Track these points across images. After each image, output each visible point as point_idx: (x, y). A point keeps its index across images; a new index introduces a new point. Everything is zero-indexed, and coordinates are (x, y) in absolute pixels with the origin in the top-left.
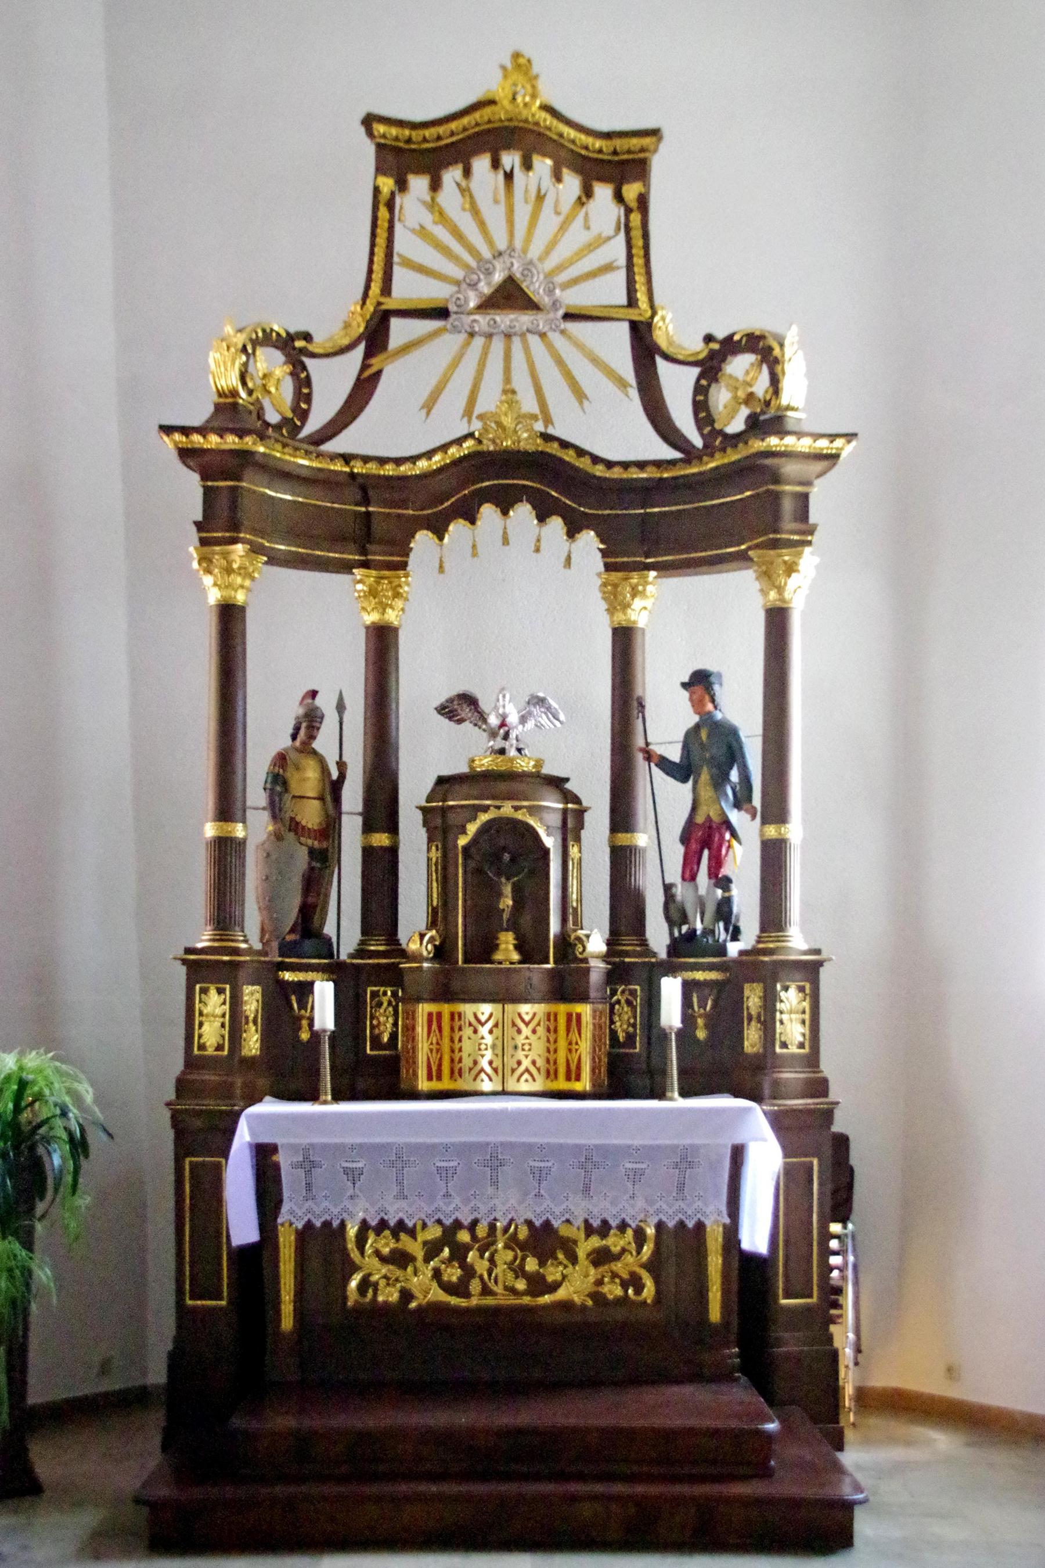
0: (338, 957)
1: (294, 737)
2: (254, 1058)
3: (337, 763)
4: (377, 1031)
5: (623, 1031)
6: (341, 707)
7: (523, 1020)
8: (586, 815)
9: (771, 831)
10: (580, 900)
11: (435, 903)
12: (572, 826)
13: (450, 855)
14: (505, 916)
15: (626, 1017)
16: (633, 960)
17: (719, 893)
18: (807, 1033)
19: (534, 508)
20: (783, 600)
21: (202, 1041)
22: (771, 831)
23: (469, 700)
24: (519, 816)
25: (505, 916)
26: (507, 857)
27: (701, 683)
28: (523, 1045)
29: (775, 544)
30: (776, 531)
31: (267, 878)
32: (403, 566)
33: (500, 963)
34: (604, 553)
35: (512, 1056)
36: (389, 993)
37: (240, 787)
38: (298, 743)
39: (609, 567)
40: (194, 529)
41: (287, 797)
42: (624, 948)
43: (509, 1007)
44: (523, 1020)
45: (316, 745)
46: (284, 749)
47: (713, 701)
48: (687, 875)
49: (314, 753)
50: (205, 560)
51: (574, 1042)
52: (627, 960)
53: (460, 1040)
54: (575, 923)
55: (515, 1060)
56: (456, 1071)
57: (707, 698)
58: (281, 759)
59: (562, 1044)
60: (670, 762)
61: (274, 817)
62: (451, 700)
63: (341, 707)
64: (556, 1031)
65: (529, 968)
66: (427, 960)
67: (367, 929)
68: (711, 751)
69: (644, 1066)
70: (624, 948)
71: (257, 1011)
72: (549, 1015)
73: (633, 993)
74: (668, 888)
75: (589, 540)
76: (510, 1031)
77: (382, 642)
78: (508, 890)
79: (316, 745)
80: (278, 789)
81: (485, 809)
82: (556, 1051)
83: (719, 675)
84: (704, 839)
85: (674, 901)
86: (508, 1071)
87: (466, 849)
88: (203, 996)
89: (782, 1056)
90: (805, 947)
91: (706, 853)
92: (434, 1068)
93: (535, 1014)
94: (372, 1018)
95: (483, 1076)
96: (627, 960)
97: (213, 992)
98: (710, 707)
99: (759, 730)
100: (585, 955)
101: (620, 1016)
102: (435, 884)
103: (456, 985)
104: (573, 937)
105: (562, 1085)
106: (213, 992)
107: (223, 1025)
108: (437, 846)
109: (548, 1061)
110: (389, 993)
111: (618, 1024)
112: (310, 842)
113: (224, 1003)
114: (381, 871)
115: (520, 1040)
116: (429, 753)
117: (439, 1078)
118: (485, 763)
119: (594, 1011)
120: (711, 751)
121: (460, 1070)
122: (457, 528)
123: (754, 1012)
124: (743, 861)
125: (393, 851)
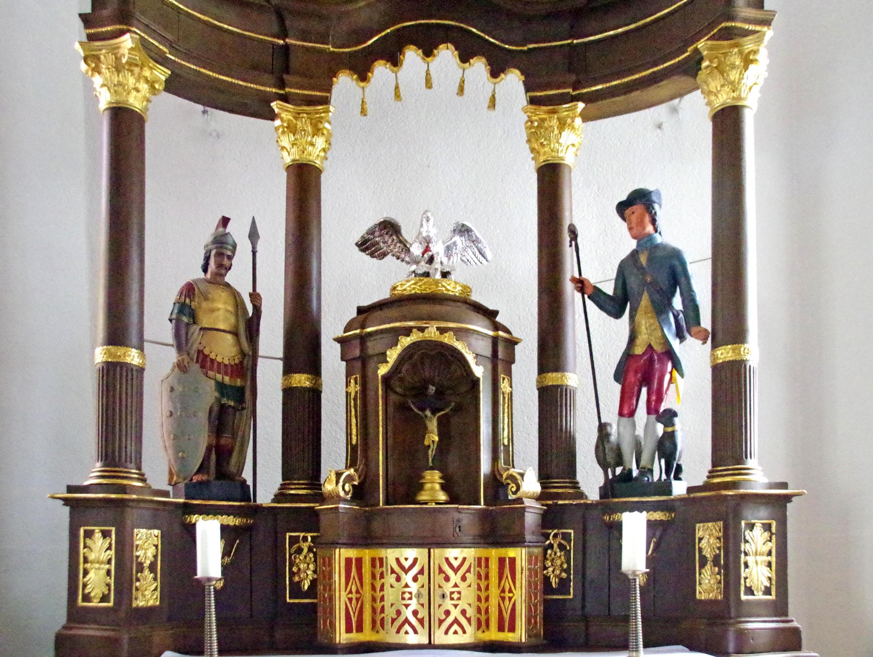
0: (255, 500)
1: (205, 269)
2: (151, 609)
3: (251, 295)
5: (556, 576)
6: (254, 235)
8: (517, 348)
9: (725, 354)
10: (511, 439)
11: (354, 442)
13: (370, 386)
14: (431, 453)
15: (559, 562)
17: (660, 429)
18: (773, 576)
20: (739, 98)
21: (87, 591)
22: (725, 354)
23: (389, 227)
24: (448, 339)
25: (431, 453)
26: (432, 389)
27: (637, 205)
29: (728, 35)
30: (731, 18)
31: (171, 414)
32: (326, 101)
33: (426, 504)
34: (528, 88)
35: (440, 606)
36: (310, 539)
37: (134, 309)
38: (209, 276)
39: (533, 101)
40: (79, 24)
41: (195, 329)
42: (555, 490)
43: (436, 552)
45: (229, 278)
46: (193, 281)
47: (654, 221)
48: (626, 412)
49: (228, 285)
50: (91, 59)
51: (507, 589)
52: (560, 502)
53: (382, 589)
54: (507, 462)
55: (443, 609)
57: (647, 219)
58: (189, 290)
59: (494, 592)
60: (605, 294)
61: (180, 348)
62: (371, 232)
63: (254, 235)
64: (487, 577)
67: (288, 473)
68: (650, 279)
70: (555, 490)
71: (155, 556)
72: (479, 559)
73: (566, 537)
74: (602, 428)
75: (513, 82)
76: (439, 579)
77: (304, 181)
78: (433, 425)
79: (229, 278)
80: (185, 319)
81: (407, 332)
82: (487, 599)
83: (658, 193)
84: (642, 372)
85: (608, 441)
86: (435, 623)
87: (386, 379)
88: (88, 541)
89: (748, 602)
90: (766, 480)
91: (644, 390)
93: (464, 559)
94: (291, 565)
95: (407, 627)
96: (560, 502)
97: (98, 535)
98: (650, 228)
99: (708, 252)
100: (519, 494)
102: (354, 421)
104: (504, 476)
105: (493, 635)
106: (98, 535)
107: (108, 572)
108: (356, 379)
109: (479, 610)
110: (310, 539)
111: (551, 569)
112: (219, 377)
113: (109, 548)
114: (302, 411)
115: (448, 588)
116: (350, 283)
117: (360, 629)
118: (410, 287)
119: (530, 556)
120: (650, 279)
121: (383, 620)
122: (381, 71)
123: (708, 554)
124: (689, 394)
125: (314, 395)
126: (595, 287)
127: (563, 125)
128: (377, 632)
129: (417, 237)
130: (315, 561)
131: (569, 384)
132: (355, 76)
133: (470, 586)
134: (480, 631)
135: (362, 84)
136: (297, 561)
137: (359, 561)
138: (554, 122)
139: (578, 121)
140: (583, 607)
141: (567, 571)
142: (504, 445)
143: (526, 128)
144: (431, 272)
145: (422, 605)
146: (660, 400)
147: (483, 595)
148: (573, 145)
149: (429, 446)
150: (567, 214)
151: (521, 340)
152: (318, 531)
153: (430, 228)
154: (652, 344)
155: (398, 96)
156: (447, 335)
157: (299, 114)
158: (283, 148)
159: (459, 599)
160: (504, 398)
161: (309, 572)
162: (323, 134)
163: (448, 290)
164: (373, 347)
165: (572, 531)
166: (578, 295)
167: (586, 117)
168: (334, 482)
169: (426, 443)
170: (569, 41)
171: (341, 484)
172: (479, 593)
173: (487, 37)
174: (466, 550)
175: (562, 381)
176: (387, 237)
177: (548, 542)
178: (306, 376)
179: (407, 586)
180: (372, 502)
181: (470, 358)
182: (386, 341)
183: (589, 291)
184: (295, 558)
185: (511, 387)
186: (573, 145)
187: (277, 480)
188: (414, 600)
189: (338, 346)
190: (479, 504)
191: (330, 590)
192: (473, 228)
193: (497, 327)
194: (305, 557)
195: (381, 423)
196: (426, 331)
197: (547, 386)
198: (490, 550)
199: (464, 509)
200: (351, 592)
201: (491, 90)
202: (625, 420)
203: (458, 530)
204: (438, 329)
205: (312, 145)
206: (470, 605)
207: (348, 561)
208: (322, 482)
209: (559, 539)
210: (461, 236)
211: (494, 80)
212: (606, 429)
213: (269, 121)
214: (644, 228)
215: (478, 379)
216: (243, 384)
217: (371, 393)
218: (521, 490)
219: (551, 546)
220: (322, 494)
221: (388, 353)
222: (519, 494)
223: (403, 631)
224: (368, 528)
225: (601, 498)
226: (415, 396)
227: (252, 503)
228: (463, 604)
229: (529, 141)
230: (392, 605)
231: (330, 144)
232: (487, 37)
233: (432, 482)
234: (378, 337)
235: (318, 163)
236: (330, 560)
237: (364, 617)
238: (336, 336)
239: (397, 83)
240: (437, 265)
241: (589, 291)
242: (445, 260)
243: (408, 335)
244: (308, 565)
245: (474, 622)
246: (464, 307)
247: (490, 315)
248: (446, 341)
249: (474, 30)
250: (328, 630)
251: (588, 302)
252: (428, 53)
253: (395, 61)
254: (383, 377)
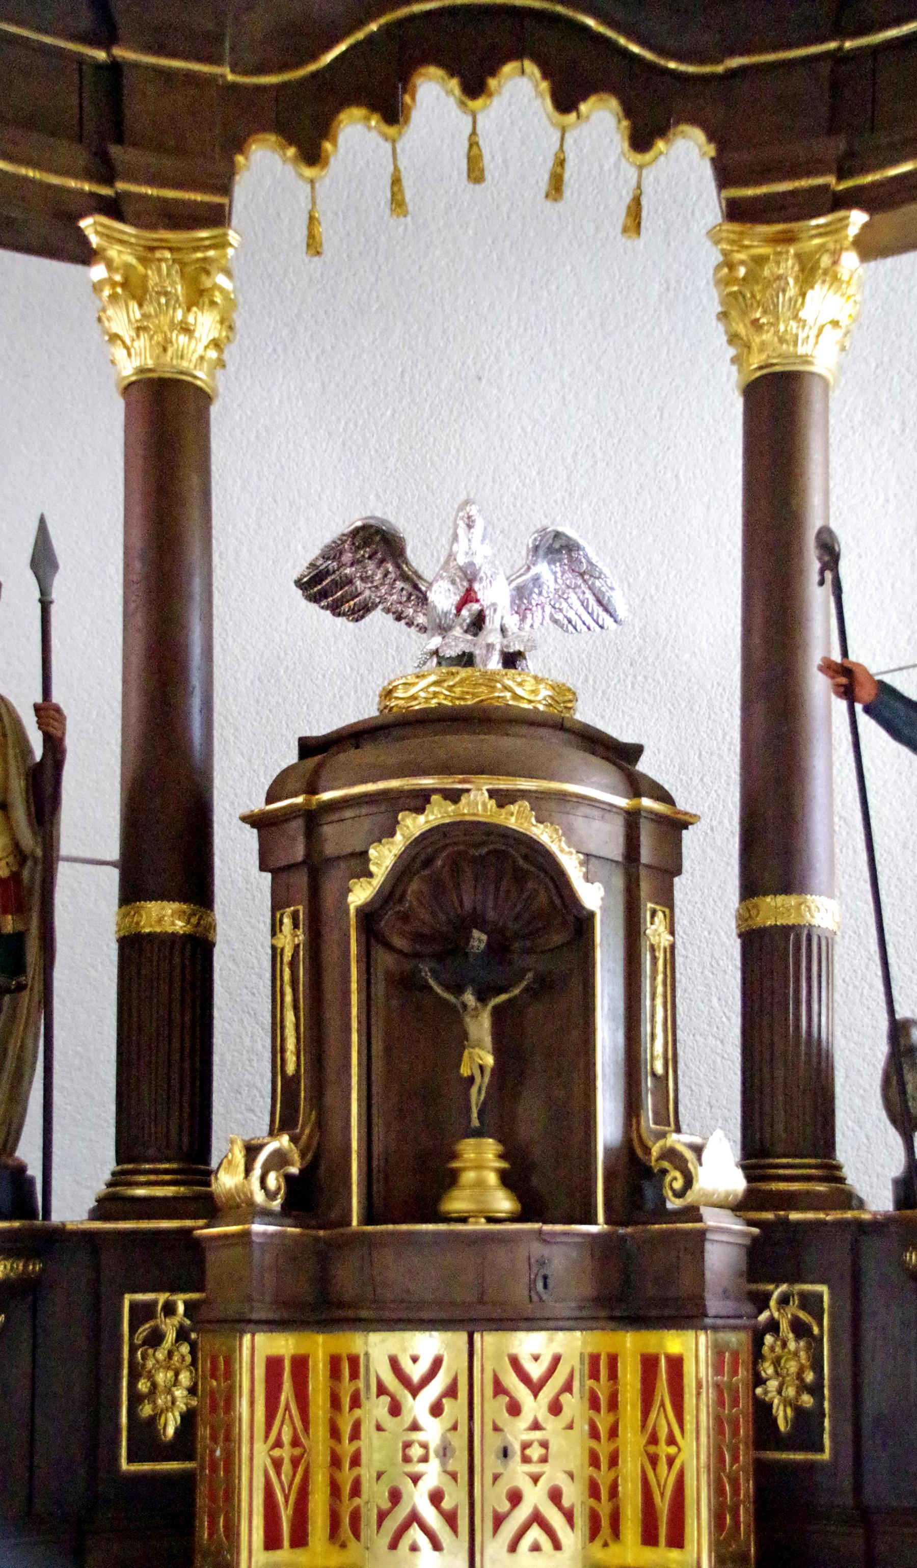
3: (37, 709)
4: (146, 1410)
5: (787, 1402)
7: (524, 1377)
8: (687, 836)
10: (672, 1059)
11: (291, 1069)
12: (651, 850)
14: (476, 1096)
16: (810, 1215)
19: (546, 74)
24: (517, 819)
25: (476, 1096)
26: (479, 939)
28: (525, 1446)
32: (217, 217)
33: (464, 1220)
34: (725, 175)
35: (496, 1478)
39: (736, 212)
42: (782, 1186)
43: (487, 1341)
44: (524, 1377)
51: (663, 1435)
52: (794, 1216)
53: (355, 1434)
54: (661, 1117)
55: (503, 1488)
56: (346, 1520)
59: (631, 1441)
62: (333, 552)
64: (613, 1405)
65: (540, 1232)
66: (265, 1214)
69: (849, 1501)
70: (782, 1186)
72: (594, 1360)
73: (811, 1303)
75: (688, 155)
76: (492, 1408)
77: (168, 427)
78: (481, 1027)
81: (419, 801)
82: (614, 1461)
86: (484, 1525)
92: (286, 1516)
93: (556, 1360)
94: (134, 1376)
95: (415, 1534)
96: (794, 1216)
100: (691, 1197)
101: (777, 1362)
102: (290, 1017)
103: (347, 1277)
104: (655, 1151)
108: (295, 917)
109: (594, 1490)
110: (181, 1308)
111: (773, 1384)
114: (167, 995)
115: (518, 1431)
116: (282, 679)
118: (424, 691)
119: (719, 1352)
121: (355, 1517)
122: (355, 134)
125: (198, 950)
126: (881, 683)
127: (809, 272)
128: (343, 1546)
129: (445, 566)
130: (194, 1363)
131: (815, 922)
132: (291, 151)
133: (570, 1427)
134: (598, 1542)
135: (309, 172)
136: (150, 1364)
137: (301, 1364)
138: (788, 266)
139: (850, 259)
140: (858, 1488)
141: (815, 1390)
142: (654, 1074)
143: (718, 283)
144: (477, 652)
145: (454, 1476)
147: (604, 1449)
148: (835, 324)
149: (471, 1079)
150: (815, 500)
151: (697, 817)
152: (200, 1288)
153: (476, 545)
155: (398, 203)
156: (514, 808)
157: (152, 249)
158: (114, 338)
159: (544, 1460)
160: (654, 959)
161: (179, 1393)
162: (213, 303)
163: (516, 697)
164: (335, 838)
165: (824, 1289)
166: (841, 705)
167: (869, 248)
168: (242, 1168)
169: (465, 1071)
170: (833, 45)
171: (257, 1172)
172: (594, 1444)
173: (622, 41)
174: (560, 1335)
175: (800, 915)
176: (371, 566)
177: (763, 1317)
178: (176, 905)
179: (415, 1427)
180: (334, 1215)
181: (571, 864)
182: (367, 823)
183: (866, 693)
184: (144, 1357)
185: (672, 933)
186: (835, 324)
187: (105, 1161)
188: (434, 1464)
189: (251, 836)
190: (593, 1221)
191: (228, 1438)
192: (582, 542)
193: (637, 785)
194: (170, 1354)
195: (354, 1024)
196: (464, 800)
198: (621, 1333)
199: (554, 1234)
200: (278, 1444)
201: (634, 183)
203: (540, 1286)
204: (492, 793)
205: (187, 330)
206: (571, 1475)
207: (274, 1365)
208: (214, 1165)
209: (793, 1309)
210: (552, 562)
211: (639, 158)
212: (908, 1035)
213: (80, 267)
215: (592, 915)
216: (21, 927)
217: (330, 954)
218: (696, 1186)
219: (773, 1326)
220: (210, 1197)
221: (372, 853)
222: (691, 1197)
223: (405, 1544)
224: (323, 1281)
226: (440, 957)
227: (39, 1222)
228: (553, 1475)
229: (724, 316)
230: (379, 1476)
231: (231, 328)
232: (622, 41)
233: (479, 1167)
234: (349, 813)
235: (202, 376)
236: (229, 1362)
237: (311, 1505)
238: (246, 811)
239: (396, 169)
240: (491, 635)
241: (866, 693)
242: (512, 622)
243: (420, 810)
244: (177, 1374)
245: (581, 1520)
246: (555, 738)
247: (622, 756)
248: (512, 823)
249: (590, 22)
250: (220, 1544)
251: (865, 722)
252: (474, 88)
253: (391, 111)
254: (360, 910)
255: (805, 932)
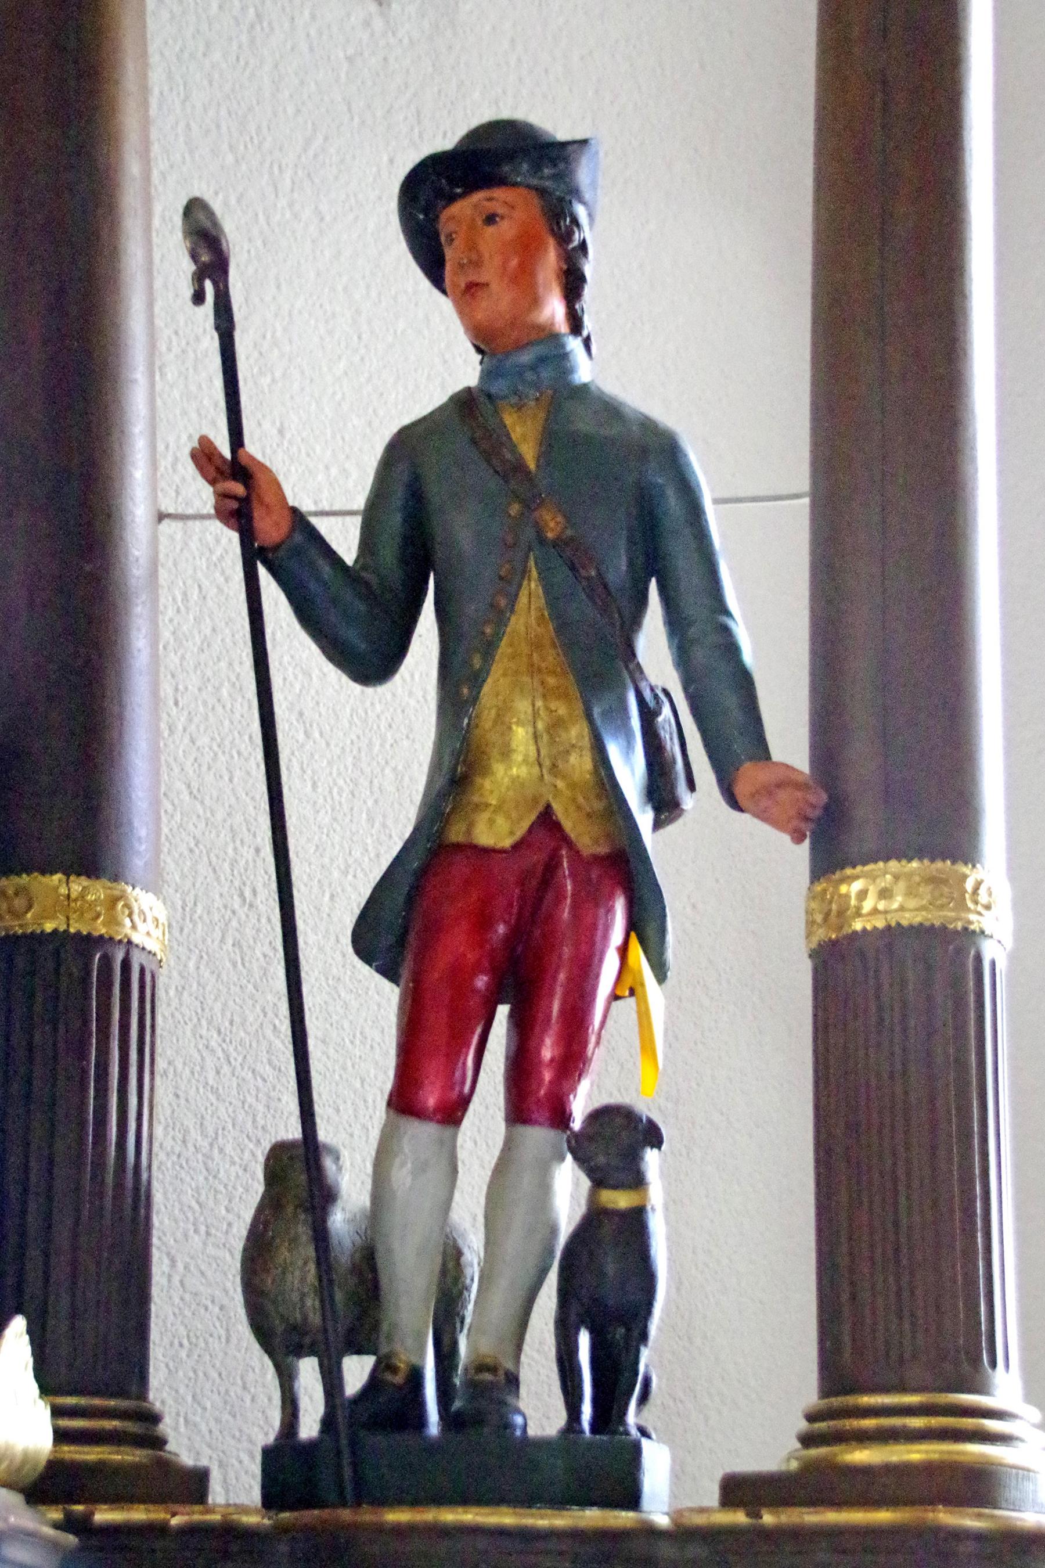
9: (879, 896)
22: (879, 896)
27: (487, 198)
47: (573, 284)
57: (550, 261)
84: (493, 936)
91: (503, 1011)
98: (554, 309)
126: (298, 518)
131: (136, 938)
146: (573, 1062)
154: (558, 808)
175: (113, 921)
197: (39, 939)
202: (420, 1134)
214: (536, 301)
225: (271, 1500)
255: (120, 956)
